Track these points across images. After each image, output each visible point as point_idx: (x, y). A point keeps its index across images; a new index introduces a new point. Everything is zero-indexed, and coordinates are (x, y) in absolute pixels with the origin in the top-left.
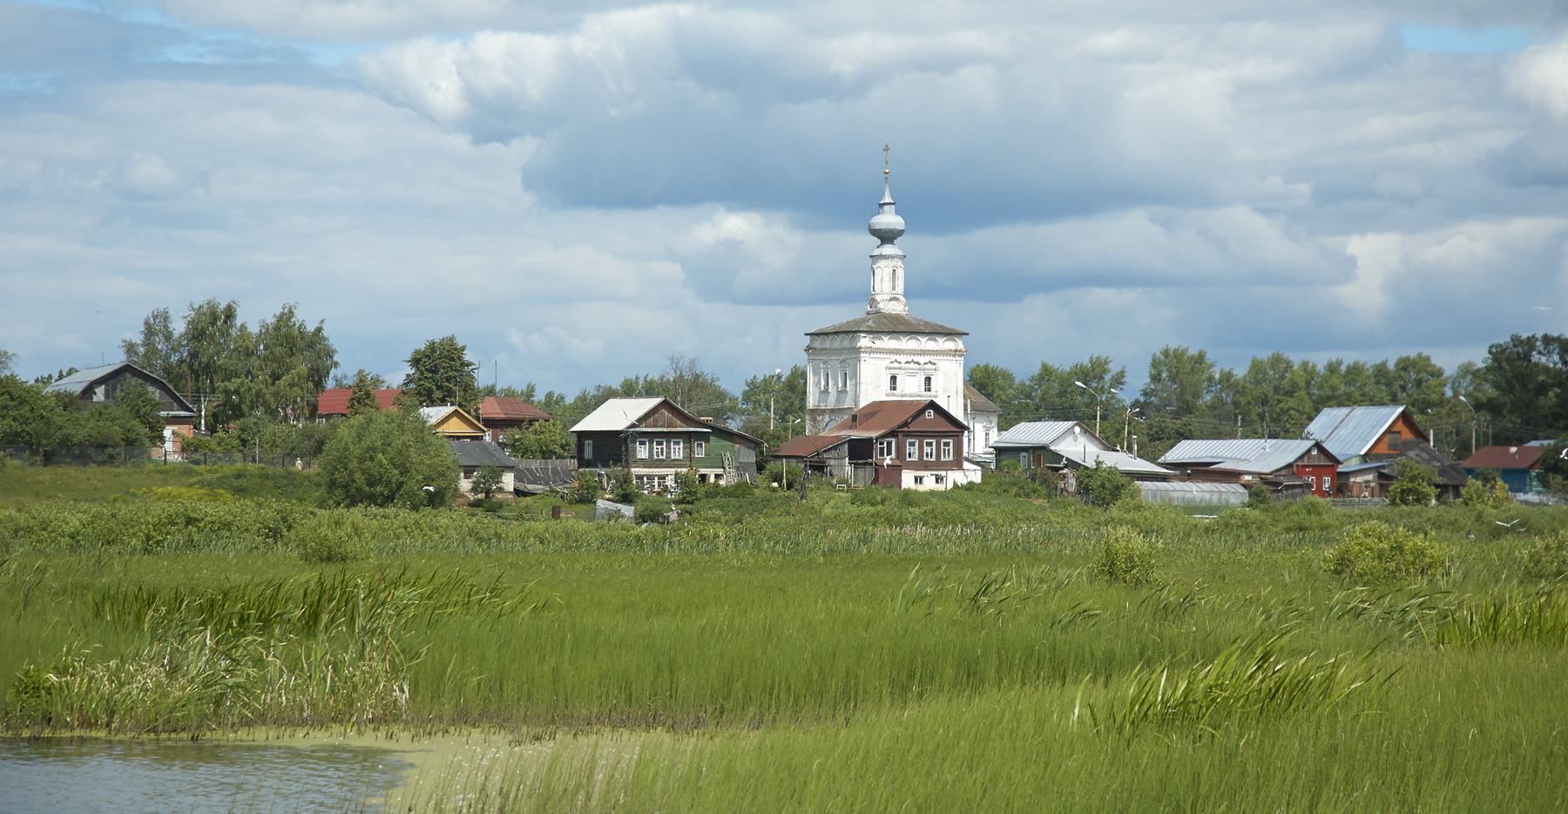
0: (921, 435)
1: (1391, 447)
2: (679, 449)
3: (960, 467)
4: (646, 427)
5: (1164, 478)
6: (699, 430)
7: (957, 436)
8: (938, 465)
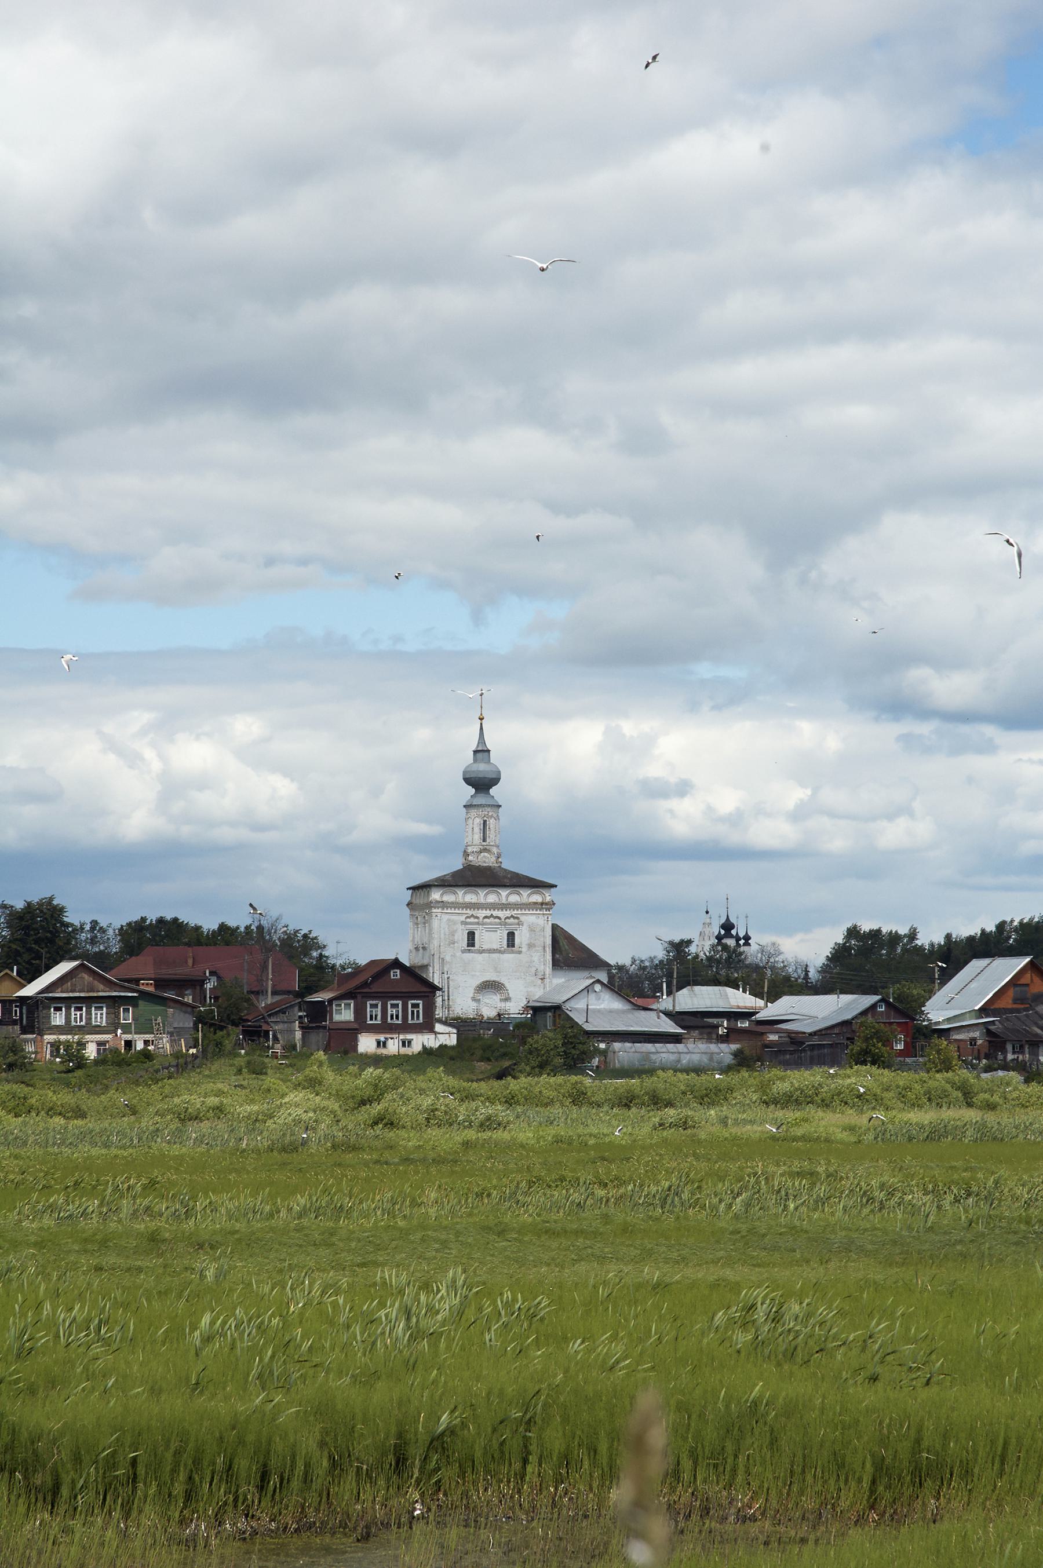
0: (385, 996)
1: (1016, 1001)
2: (102, 1014)
3: (431, 1030)
4: (62, 992)
5: (676, 1039)
6: (123, 994)
7: (428, 996)
8: (406, 1027)
